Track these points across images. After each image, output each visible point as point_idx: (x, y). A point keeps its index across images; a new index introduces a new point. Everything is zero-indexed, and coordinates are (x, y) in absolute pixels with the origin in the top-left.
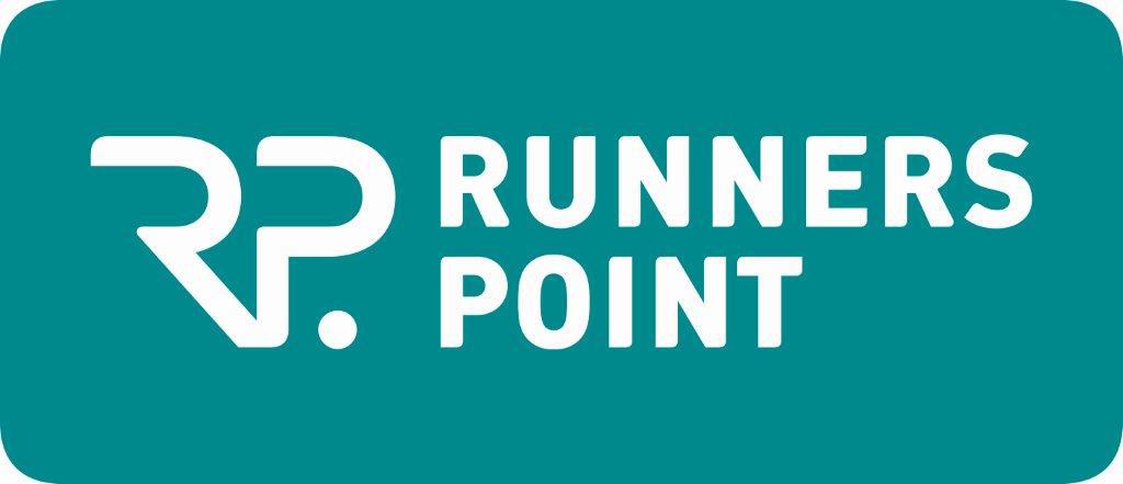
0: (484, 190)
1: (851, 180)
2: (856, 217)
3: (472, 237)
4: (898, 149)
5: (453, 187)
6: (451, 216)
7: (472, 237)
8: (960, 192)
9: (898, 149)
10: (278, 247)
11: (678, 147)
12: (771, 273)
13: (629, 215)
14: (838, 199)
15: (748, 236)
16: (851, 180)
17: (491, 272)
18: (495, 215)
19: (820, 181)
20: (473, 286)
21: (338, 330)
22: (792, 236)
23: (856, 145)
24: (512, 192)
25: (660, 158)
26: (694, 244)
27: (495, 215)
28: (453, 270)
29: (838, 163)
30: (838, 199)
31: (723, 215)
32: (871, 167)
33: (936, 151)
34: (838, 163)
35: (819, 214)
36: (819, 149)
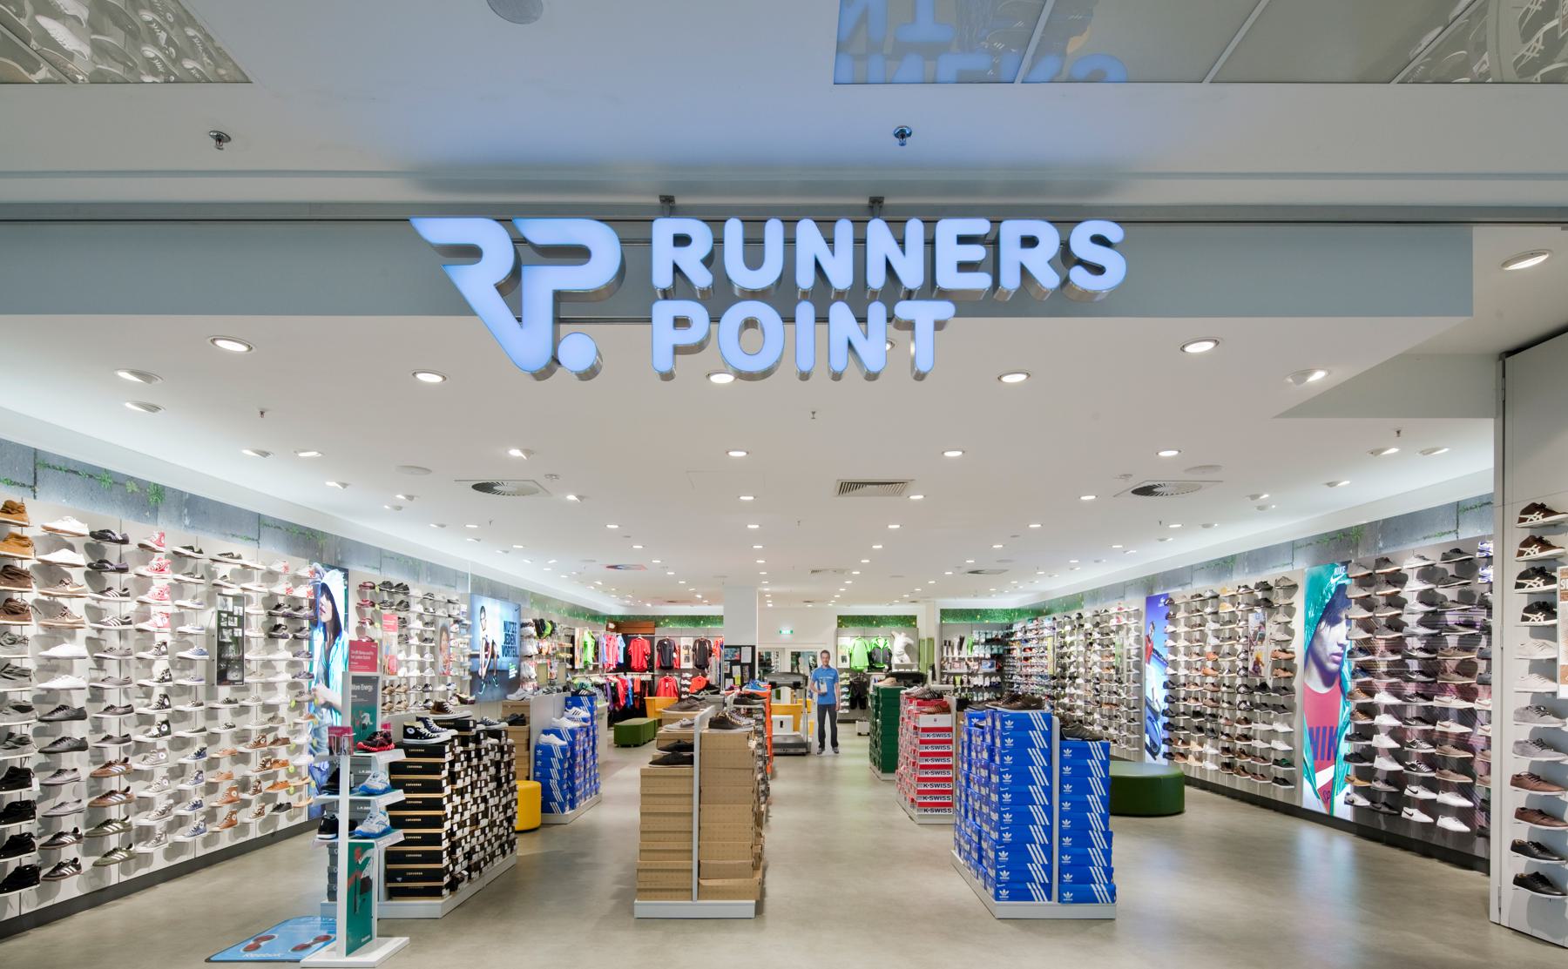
0: (691, 260)
1: (977, 253)
4: (1012, 231)
5: (663, 256)
6: (662, 278)
9: (1012, 231)
13: (844, 230)
14: (964, 267)
16: (977, 253)
17: (697, 312)
18: (701, 278)
19: (949, 253)
20: (681, 322)
23: (981, 226)
24: (711, 261)
25: (862, 320)
27: (701, 278)
28: (664, 311)
31: (876, 279)
33: (1049, 237)
35: (948, 278)
36: (948, 230)
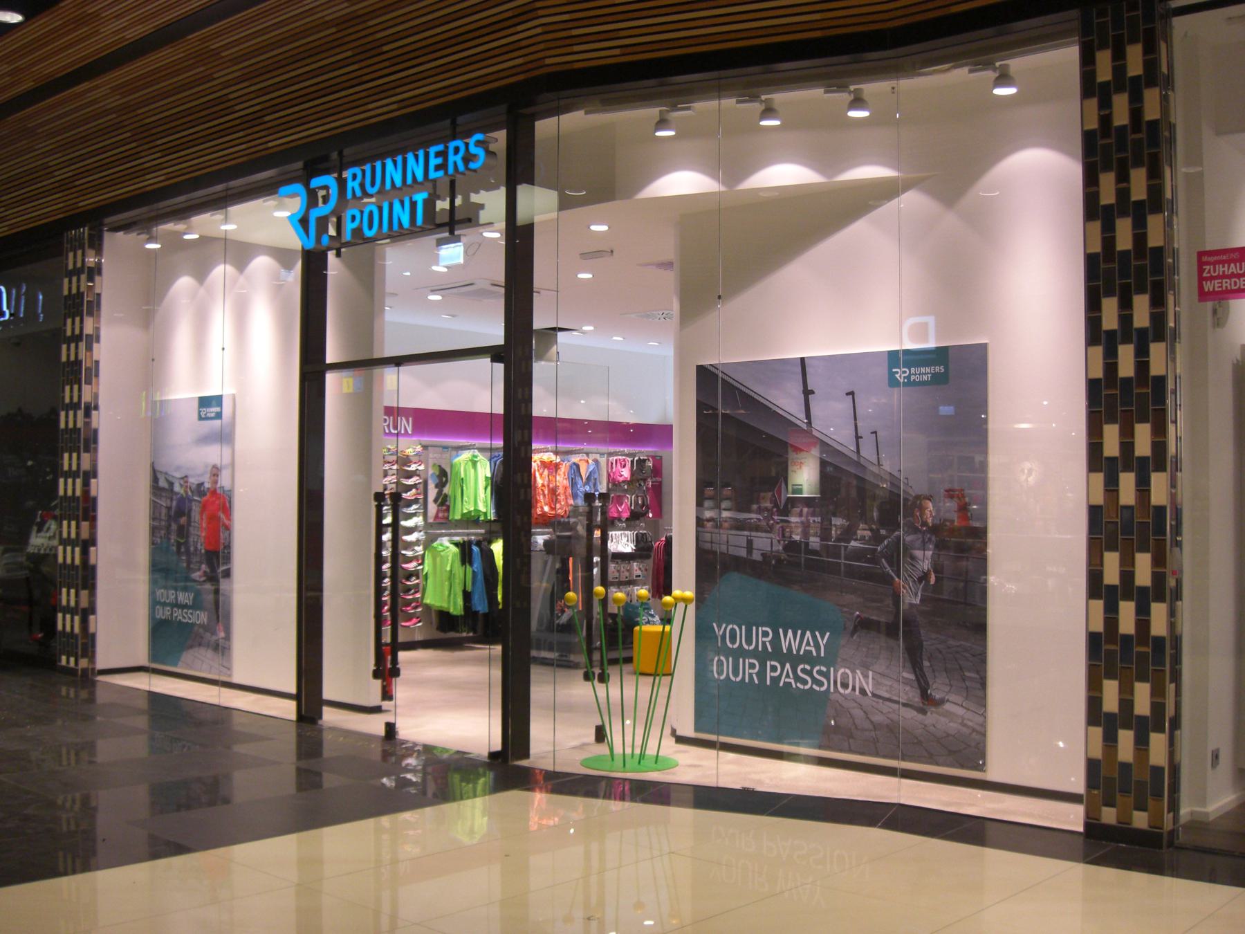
2: (1220, 289)
3: (913, 374)
7: (913, 374)
8: (940, 370)
10: (903, 375)
11: (421, 153)
12: (929, 375)
14: (1219, 287)
15: (928, 373)
16: (1220, 285)
19: (1217, 285)
21: (906, 380)
22: (931, 373)
23: (440, 148)
26: (925, 374)
29: (1218, 283)
30: (1219, 287)
32: (1221, 283)
34: (1218, 283)
36: (433, 150)
